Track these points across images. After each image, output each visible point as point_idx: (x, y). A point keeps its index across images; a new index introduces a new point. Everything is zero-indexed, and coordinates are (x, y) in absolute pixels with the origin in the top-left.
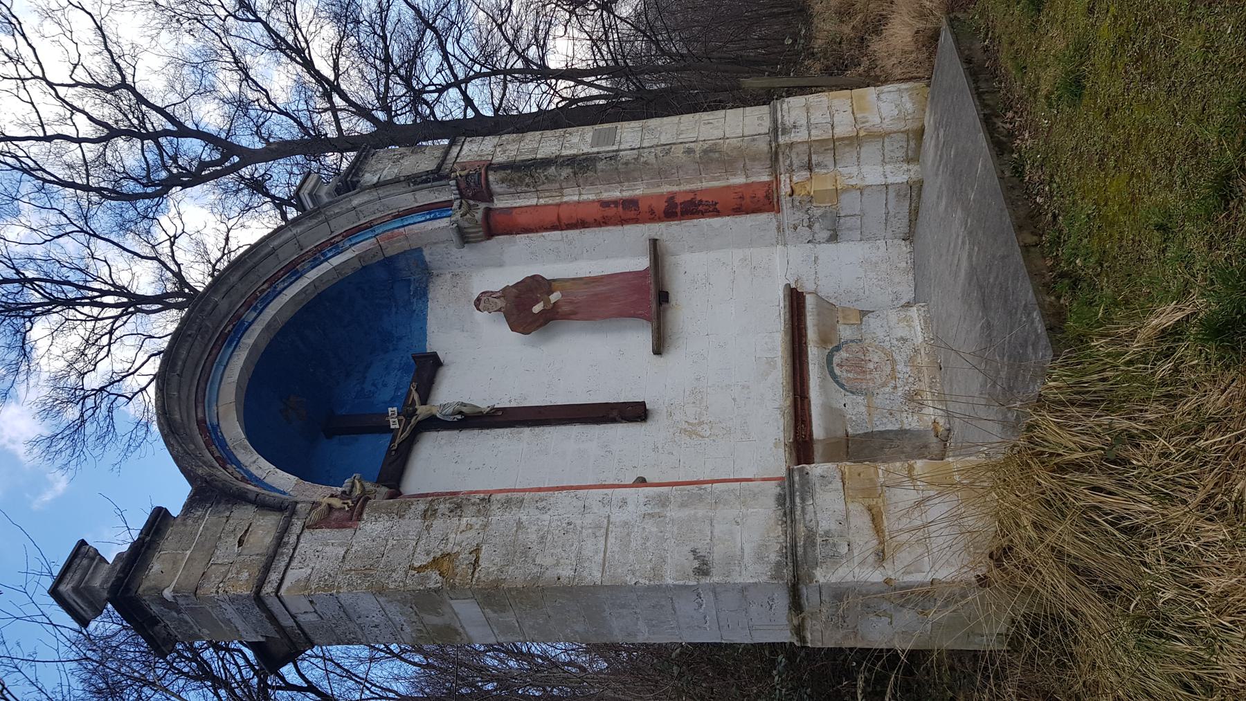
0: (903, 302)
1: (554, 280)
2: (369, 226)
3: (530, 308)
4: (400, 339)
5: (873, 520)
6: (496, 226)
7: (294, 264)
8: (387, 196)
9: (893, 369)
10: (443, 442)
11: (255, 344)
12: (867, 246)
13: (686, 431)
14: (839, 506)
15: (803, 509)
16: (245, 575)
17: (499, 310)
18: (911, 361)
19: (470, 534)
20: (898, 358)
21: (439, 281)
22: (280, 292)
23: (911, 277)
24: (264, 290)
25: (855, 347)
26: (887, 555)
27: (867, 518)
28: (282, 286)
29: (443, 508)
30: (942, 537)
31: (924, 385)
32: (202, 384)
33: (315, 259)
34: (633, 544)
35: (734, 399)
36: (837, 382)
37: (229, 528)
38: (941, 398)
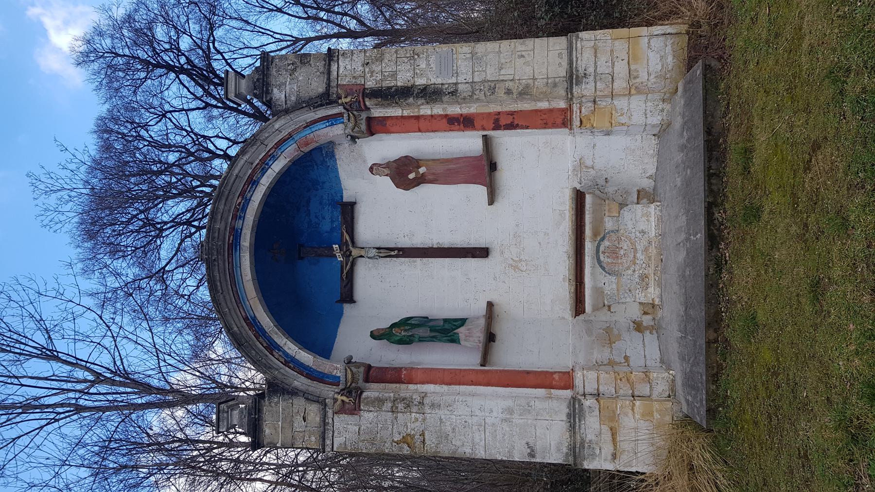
0: (648, 175)
2: (290, 136)
3: (405, 173)
4: (324, 183)
5: (613, 435)
6: (374, 127)
10: (370, 265)
12: (629, 138)
15: (580, 426)
16: (313, 438)
18: (646, 249)
19: (418, 424)
20: (638, 247)
21: (341, 148)
23: (655, 159)
26: (618, 456)
28: (249, 195)
29: (401, 406)
30: (644, 448)
31: (650, 271)
36: (601, 266)
37: (295, 411)
38: (659, 284)
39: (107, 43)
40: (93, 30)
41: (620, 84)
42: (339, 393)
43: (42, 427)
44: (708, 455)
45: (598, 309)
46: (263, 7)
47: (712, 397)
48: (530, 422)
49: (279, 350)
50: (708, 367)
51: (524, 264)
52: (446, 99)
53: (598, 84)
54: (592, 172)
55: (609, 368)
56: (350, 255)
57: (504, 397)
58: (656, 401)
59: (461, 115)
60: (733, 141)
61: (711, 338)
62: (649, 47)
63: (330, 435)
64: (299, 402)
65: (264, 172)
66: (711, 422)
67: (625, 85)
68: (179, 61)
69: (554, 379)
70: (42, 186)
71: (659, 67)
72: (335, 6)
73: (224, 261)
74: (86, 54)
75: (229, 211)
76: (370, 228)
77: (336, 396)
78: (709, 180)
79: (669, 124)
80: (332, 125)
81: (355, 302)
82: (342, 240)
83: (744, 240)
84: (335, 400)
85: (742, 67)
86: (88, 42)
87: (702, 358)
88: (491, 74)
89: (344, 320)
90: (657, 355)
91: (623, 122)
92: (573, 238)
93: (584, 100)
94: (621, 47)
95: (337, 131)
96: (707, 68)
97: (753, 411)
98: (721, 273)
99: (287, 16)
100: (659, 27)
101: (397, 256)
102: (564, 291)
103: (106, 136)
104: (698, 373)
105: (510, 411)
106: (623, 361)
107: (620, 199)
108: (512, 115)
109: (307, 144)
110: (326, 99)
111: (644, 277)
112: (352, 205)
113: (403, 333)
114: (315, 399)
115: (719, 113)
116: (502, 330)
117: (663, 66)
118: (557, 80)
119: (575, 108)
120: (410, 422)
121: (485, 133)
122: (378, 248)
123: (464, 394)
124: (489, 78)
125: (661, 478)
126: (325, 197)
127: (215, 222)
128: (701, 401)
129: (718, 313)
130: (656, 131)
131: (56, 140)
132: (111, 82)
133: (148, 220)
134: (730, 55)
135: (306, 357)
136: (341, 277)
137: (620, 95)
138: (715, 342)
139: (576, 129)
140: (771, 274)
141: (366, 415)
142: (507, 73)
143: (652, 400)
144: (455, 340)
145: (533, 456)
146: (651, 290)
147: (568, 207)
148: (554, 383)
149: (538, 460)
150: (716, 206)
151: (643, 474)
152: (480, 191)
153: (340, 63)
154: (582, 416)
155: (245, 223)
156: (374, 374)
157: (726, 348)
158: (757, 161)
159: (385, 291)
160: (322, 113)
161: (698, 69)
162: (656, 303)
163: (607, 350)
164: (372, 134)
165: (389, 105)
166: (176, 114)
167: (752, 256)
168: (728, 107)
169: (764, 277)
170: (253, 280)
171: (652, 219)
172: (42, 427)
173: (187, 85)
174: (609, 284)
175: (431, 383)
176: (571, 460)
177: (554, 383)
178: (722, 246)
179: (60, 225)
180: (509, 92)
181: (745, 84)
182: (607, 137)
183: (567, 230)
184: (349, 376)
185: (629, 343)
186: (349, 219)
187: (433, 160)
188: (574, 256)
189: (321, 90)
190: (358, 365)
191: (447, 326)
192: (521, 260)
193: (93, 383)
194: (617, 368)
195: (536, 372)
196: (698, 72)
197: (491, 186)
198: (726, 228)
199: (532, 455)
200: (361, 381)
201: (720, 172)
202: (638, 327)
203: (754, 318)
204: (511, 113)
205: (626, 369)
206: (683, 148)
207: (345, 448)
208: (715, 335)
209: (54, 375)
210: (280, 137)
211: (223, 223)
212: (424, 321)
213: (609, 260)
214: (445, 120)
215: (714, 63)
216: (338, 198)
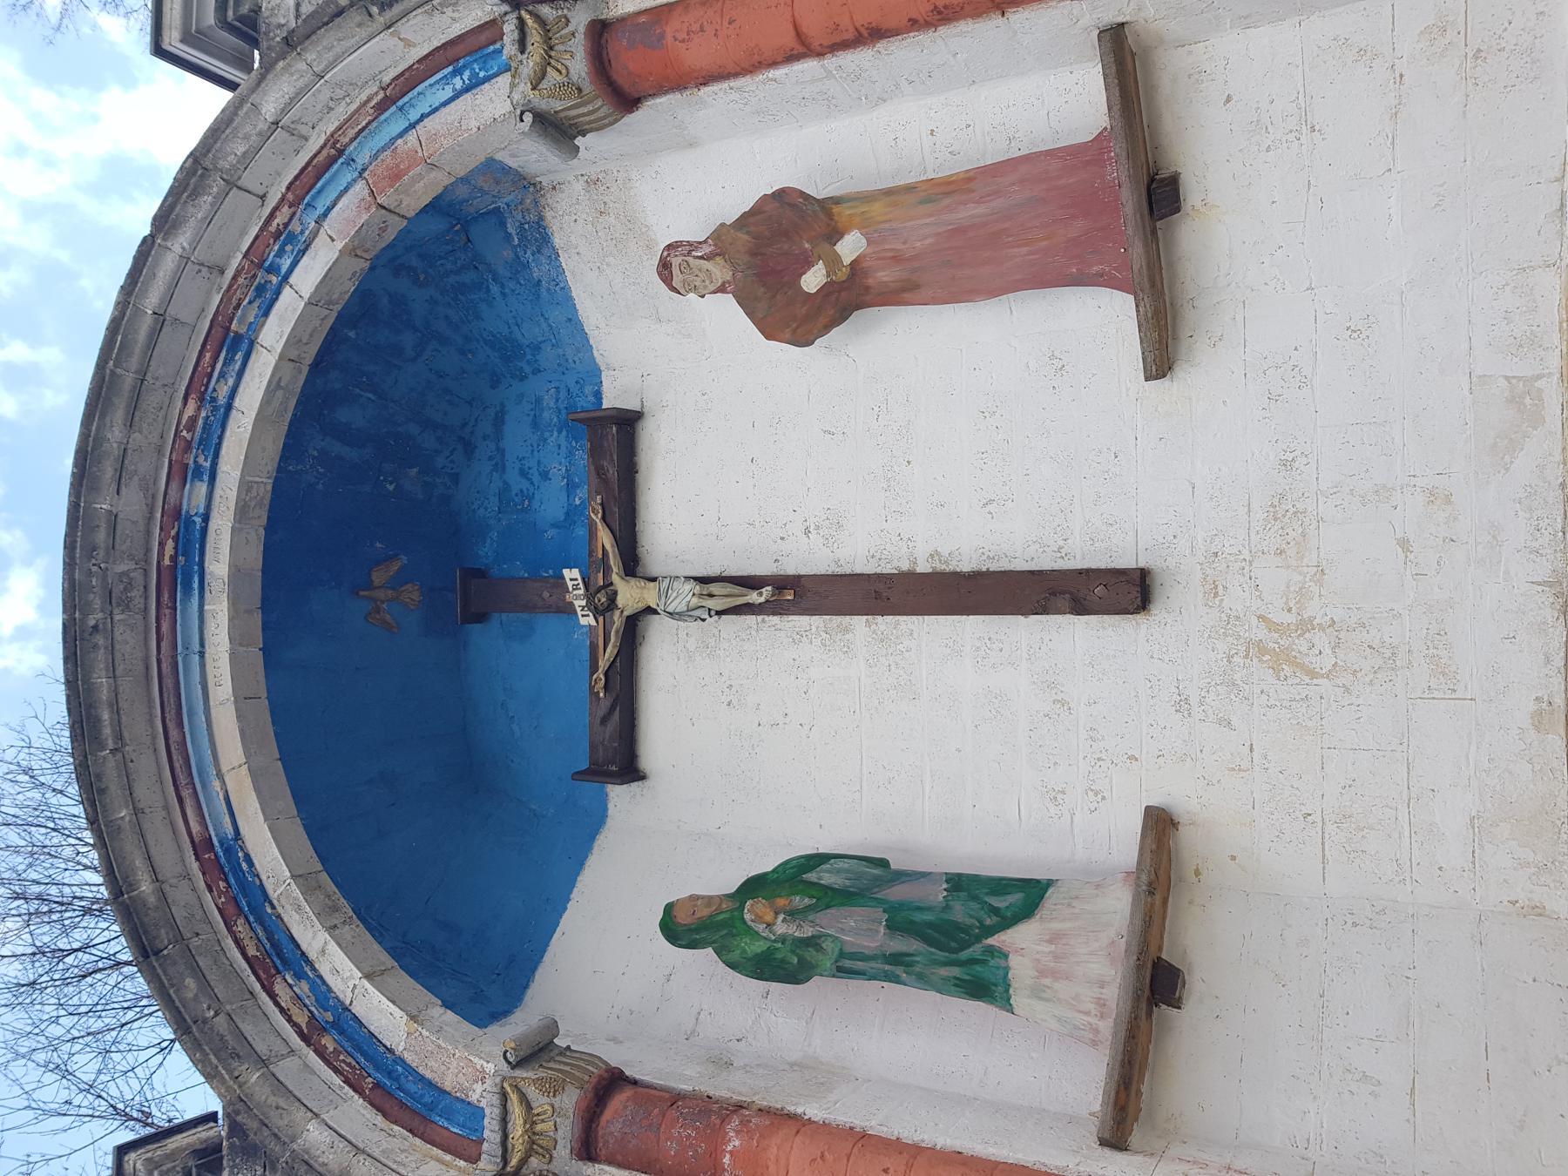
1: (837, 201)
2: (334, 154)
3: (789, 268)
4: (537, 348)
8: (331, 65)
11: (236, 571)
13: (1262, 650)
17: (721, 289)
22: (229, 407)
24: (191, 426)
28: (223, 391)
33: (261, 290)
35: (1404, 544)
49: (299, 976)
51: (1321, 640)
65: (267, 299)
75: (160, 451)
76: (694, 509)
82: (591, 553)
101: (772, 608)
112: (628, 422)
116: (1208, 943)
122: (696, 579)
126: (549, 401)
127: (95, 488)
144: (984, 985)
152: (1106, 318)
155: (218, 492)
159: (754, 748)
164: (627, 102)
187: (889, 192)
191: (961, 912)
192: (1305, 626)
200: (563, 1152)
216: (585, 402)
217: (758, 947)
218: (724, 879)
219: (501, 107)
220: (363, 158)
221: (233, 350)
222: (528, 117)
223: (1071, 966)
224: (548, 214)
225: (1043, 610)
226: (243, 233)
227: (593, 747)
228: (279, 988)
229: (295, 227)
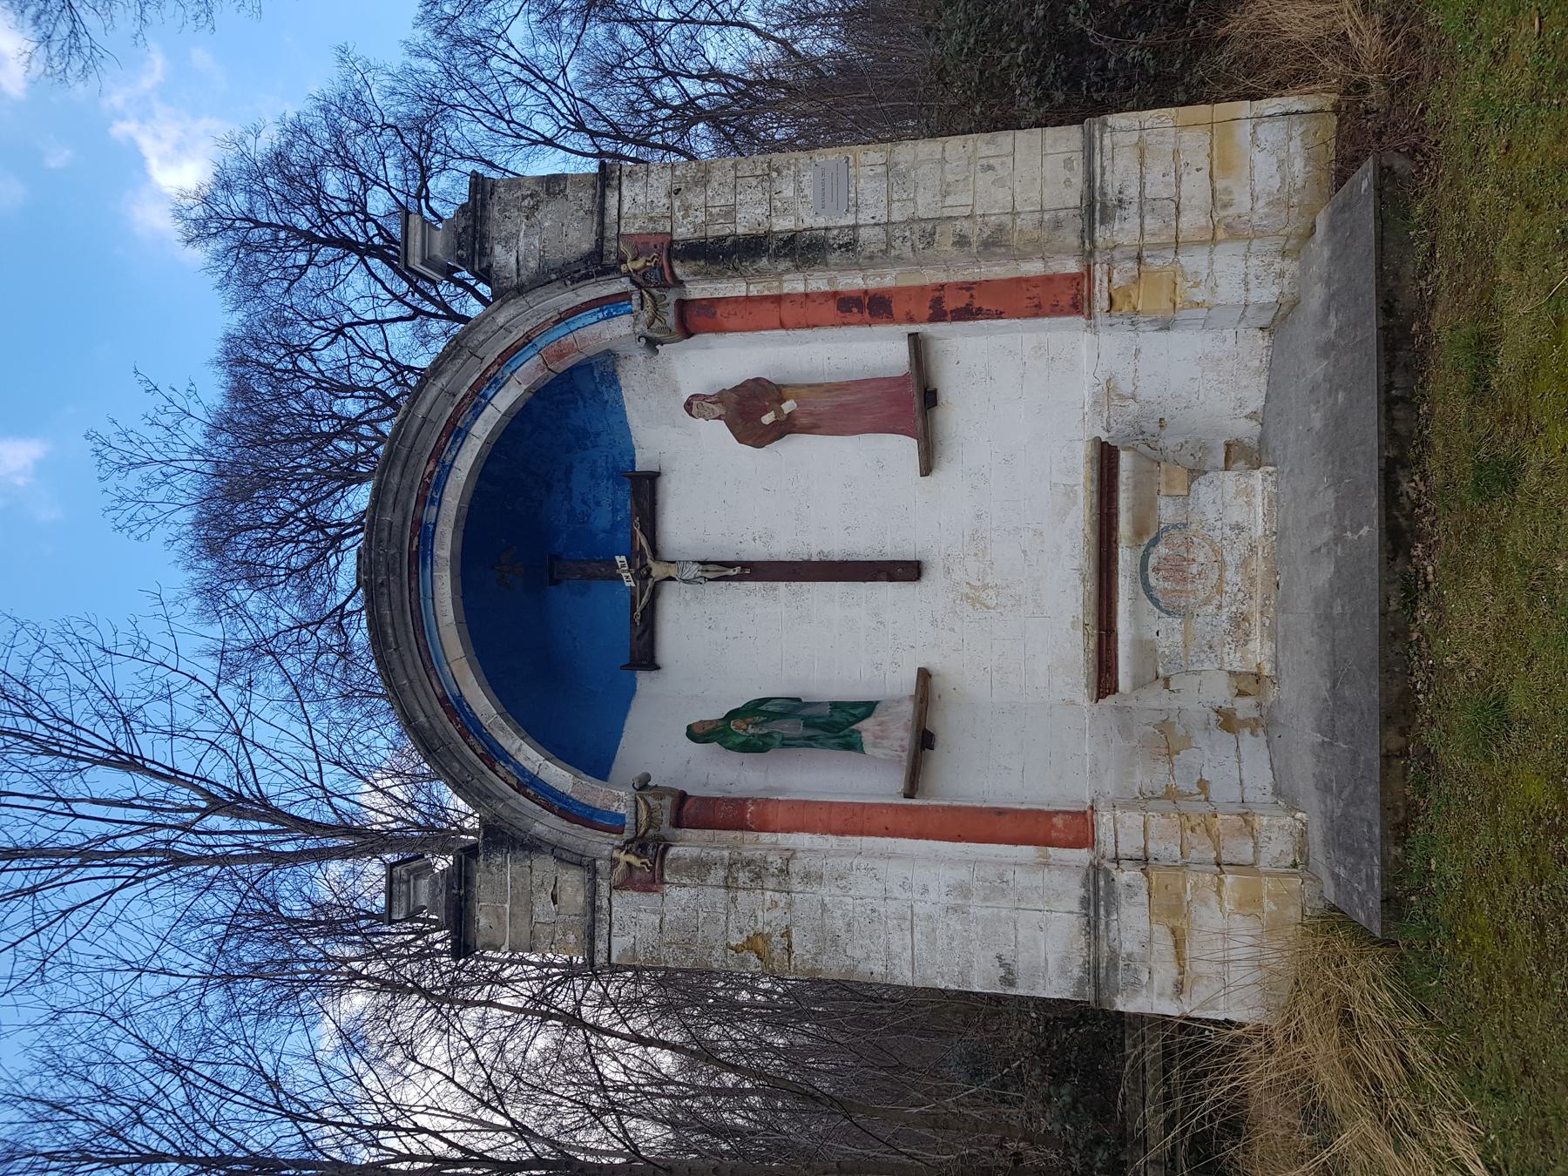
0: (1248, 411)
2: (528, 340)
3: (754, 413)
4: (598, 435)
6: (693, 321)
7: (452, 421)
9: (1220, 577)
10: (688, 597)
12: (1210, 336)
14: (1143, 924)
17: (719, 418)
18: (1244, 564)
19: (777, 913)
20: (1228, 559)
23: (1263, 379)
24: (432, 473)
25: (1177, 538)
27: (1170, 942)
28: (449, 457)
29: (743, 877)
30: (1240, 974)
31: (1254, 607)
32: (421, 641)
34: (939, 943)
35: (1024, 552)
36: (1151, 598)
38: (1272, 634)
39: (240, 201)
40: (214, 179)
41: (1193, 220)
42: (621, 849)
43: (113, 892)
44: (1387, 996)
45: (1143, 686)
46: (519, 136)
47: (1394, 873)
48: (1004, 913)
50: (1386, 808)
51: (992, 593)
52: (833, 258)
53: (1148, 220)
54: (1133, 407)
55: (1167, 805)
56: (649, 575)
57: (952, 862)
58: (1268, 874)
59: (866, 292)
60: (1447, 325)
61: (1393, 746)
62: (1254, 141)
63: (605, 932)
64: (544, 866)
65: (478, 410)
66: (1392, 925)
67: (1203, 221)
68: (366, 232)
69: (1053, 826)
70: (115, 457)
71: (1276, 183)
72: (650, 135)
73: (402, 586)
74: (201, 224)
75: (411, 489)
76: (687, 524)
77: (616, 854)
78: (1388, 411)
79: (1295, 304)
80: (610, 316)
81: (658, 668)
83: (1472, 537)
84: (615, 862)
85: (1468, 161)
86: (205, 200)
87: (1373, 789)
88: (925, 204)
89: (637, 703)
90: (1265, 778)
91: (1199, 299)
92: (1093, 539)
93: (1117, 254)
94: (1195, 144)
95: (618, 330)
96: (1384, 174)
97: (1494, 908)
98: (1415, 609)
99: (561, 153)
100: (1276, 101)
102: (1076, 648)
103: (240, 370)
104: (1362, 819)
105: (964, 890)
106: (1196, 790)
107: (1191, 463)
108: (968, 289)
109: (561, 356)
110: (596, 264)
111: (1239, 620)
112: (653, 477)
113: (751, 730)
114: (575, 859)
115: (1410, 270)
116: (946, 724)
117: (1283, 179)
118: (1062, 214)
119: (1099, 272)
120: (760, 909)
121: (914, 328)
123: (872, 855)
124: (922, 213)
125: (1278, 1037)
128: (1369, 878)
129: (1409, 693)
130: (1266, 319)
131: (136, 372)
132: (245, 272)
133: (314, 520)
134: (1437, 143)
135: (559, 776)
136: (632, 619)
137: (1194, 243)
138: (1401, 756)
139: (1101, 318)
140: (1546, 608)
141: (675, 893)
142: (959, 202)
143: (1258, 873)
145: (1012, 984)
146: (1255, 645)
147: (1081, 479)
148: (1054, 834)
149: (1021, 992)
150: (1404, 466)
151: (1241, 1026)
152: (905, 448)
153: (625, 192)
154: (1112, 902)
156: (691, 811)
157: (1426, 768)
158: (1508, 361)
159: (719, 647)
160: (589, 292)
161: (1364, 179)
162: (1266, 672)
163: (1162, 769)
164: (689, 335)
165: (721, 275)
166: (362, 329)
167: (1495, 573)
168: (1432, 255)
169: (1528, 615)
170: (458, 623)
171: (1258, 500)
172: (113, 892)
173: (382, 277)
174: (1168, 634)
175: (804, 831)
176: (1089, 994)
177: (1054, 834)
178: (1418, 550)
179: (147, 527)
180: (962, 241)
181: (1477, 198)
182: (1162, 334)
183: (1081, 525)
184: (643, 815)
185: (1208, 754)
186: (646, 505)
188: (1095, 576)
189: (587, 246)
190: (661, 793)
191: (837, 717)
192: (986, 587)
193: (205, 813)
194: (1184, 805)
195: (1016, 811)
196: (1365, 184)
197: (926, 436)
198: (1427, 512)
199: (1008, 980)
200: (666, 825)
201: (1414, 395)
202: (1227, 721)
203: (1499, 706)
204: (968, 287)
205: (1203, 807)
206: (1325, 350)
207: (635, 958)
208: (1402, 740)
209: (138, 797)
210: (508, 342)
211: (399, 512)
212: (793, 707)
213: (1168, 585)
214: (832, 304)
215: (1400, 163)
216: (624, 465)
217: (741, 739)
218: (718, 713)
219: (628, 331)
220: (540, 345)
221: (457, 437)
222: (643, 340)
223: (888, 737)
224: (620, 369)
225: (875, 580)
226: (469, 376)
227: (632, 652)
228: (498, 768)
229: (499, 375)
